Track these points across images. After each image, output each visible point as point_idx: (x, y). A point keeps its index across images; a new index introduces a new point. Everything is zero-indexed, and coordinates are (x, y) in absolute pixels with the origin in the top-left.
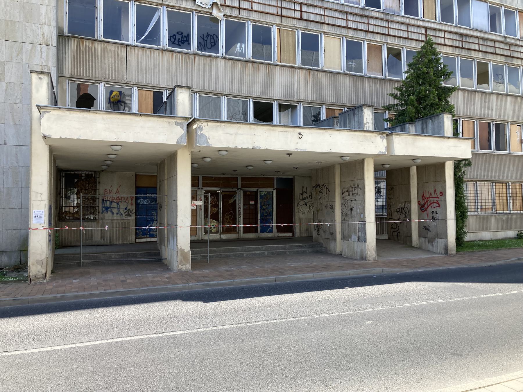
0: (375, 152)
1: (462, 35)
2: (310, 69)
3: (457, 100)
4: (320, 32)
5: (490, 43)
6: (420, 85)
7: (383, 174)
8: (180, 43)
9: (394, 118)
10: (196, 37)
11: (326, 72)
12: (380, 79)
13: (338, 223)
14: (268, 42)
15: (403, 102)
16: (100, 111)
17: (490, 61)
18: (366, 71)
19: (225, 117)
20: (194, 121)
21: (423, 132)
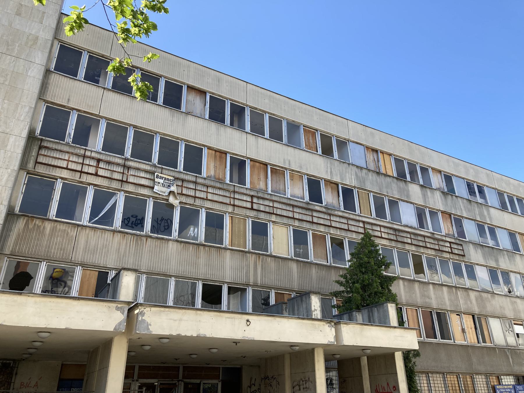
0: (325, 342)
1: (395, 230)
2: (259, 254)
3: (399, 289)
4: (269, 221)
5: (420, 238)
6: (363, 274)
7: (335, 364)
8: (133, 226)
9: (341, 305)
10: (150, 221)
11: (275, 257)
12: (326, 266)
14: (220, 226)
15: (349, 289)
16: (34, 293)
17: (423, 253)
18: (311, 258)
19: (171, 303)
20: (137, 306)
21: (370, 322)
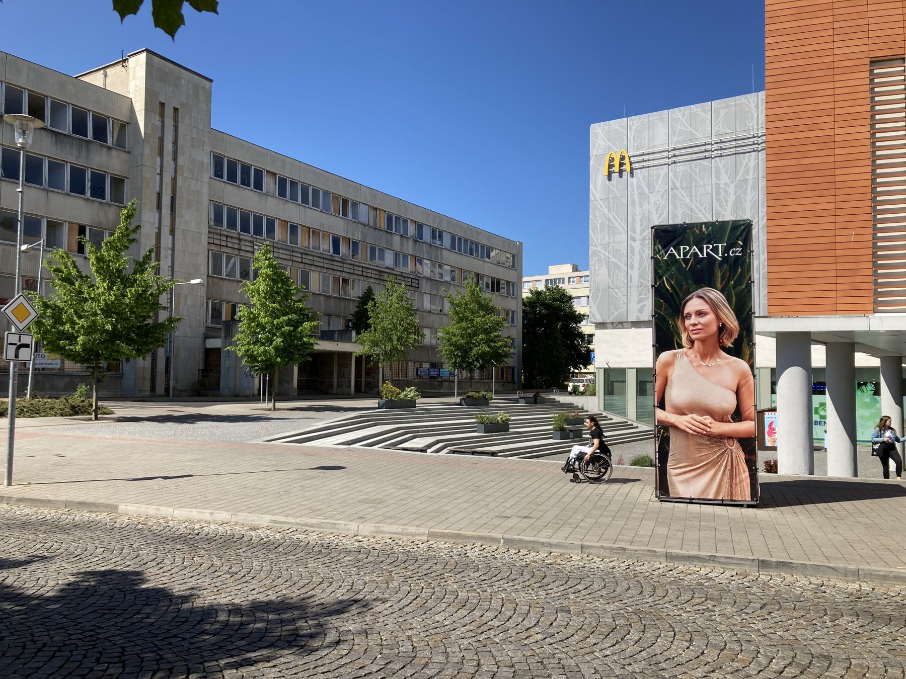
1: (380, 271)
13: (335, 379)
